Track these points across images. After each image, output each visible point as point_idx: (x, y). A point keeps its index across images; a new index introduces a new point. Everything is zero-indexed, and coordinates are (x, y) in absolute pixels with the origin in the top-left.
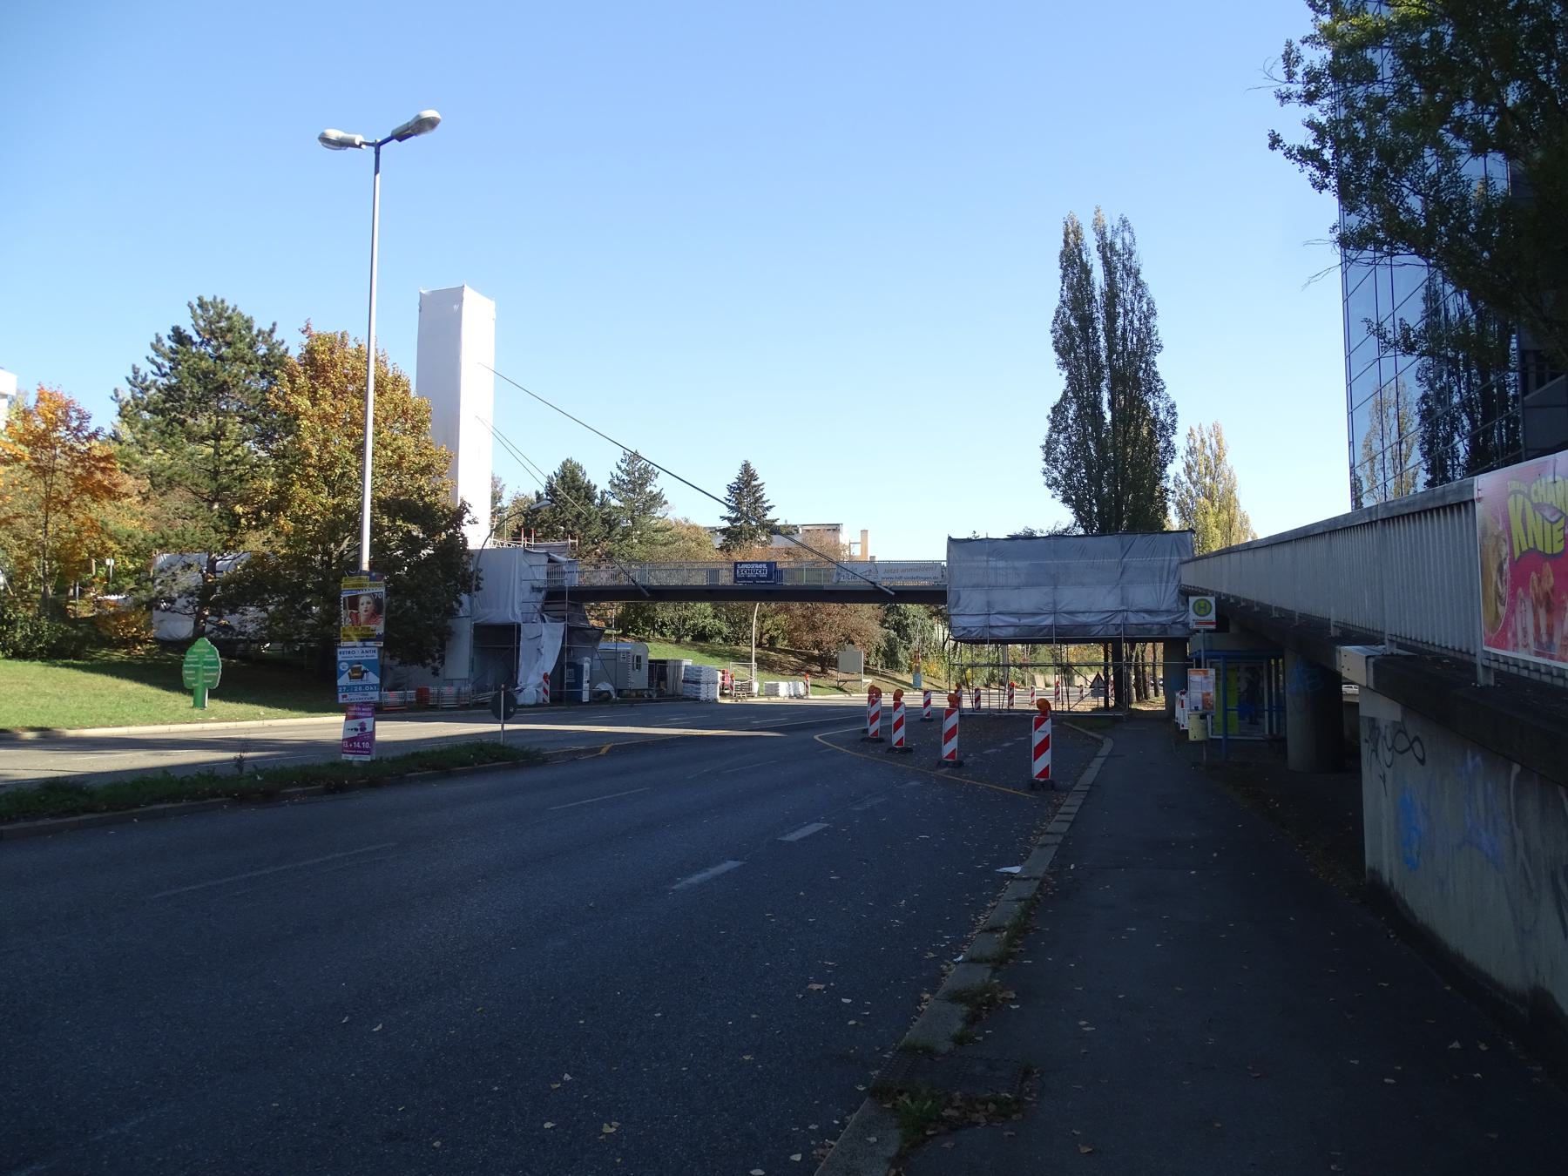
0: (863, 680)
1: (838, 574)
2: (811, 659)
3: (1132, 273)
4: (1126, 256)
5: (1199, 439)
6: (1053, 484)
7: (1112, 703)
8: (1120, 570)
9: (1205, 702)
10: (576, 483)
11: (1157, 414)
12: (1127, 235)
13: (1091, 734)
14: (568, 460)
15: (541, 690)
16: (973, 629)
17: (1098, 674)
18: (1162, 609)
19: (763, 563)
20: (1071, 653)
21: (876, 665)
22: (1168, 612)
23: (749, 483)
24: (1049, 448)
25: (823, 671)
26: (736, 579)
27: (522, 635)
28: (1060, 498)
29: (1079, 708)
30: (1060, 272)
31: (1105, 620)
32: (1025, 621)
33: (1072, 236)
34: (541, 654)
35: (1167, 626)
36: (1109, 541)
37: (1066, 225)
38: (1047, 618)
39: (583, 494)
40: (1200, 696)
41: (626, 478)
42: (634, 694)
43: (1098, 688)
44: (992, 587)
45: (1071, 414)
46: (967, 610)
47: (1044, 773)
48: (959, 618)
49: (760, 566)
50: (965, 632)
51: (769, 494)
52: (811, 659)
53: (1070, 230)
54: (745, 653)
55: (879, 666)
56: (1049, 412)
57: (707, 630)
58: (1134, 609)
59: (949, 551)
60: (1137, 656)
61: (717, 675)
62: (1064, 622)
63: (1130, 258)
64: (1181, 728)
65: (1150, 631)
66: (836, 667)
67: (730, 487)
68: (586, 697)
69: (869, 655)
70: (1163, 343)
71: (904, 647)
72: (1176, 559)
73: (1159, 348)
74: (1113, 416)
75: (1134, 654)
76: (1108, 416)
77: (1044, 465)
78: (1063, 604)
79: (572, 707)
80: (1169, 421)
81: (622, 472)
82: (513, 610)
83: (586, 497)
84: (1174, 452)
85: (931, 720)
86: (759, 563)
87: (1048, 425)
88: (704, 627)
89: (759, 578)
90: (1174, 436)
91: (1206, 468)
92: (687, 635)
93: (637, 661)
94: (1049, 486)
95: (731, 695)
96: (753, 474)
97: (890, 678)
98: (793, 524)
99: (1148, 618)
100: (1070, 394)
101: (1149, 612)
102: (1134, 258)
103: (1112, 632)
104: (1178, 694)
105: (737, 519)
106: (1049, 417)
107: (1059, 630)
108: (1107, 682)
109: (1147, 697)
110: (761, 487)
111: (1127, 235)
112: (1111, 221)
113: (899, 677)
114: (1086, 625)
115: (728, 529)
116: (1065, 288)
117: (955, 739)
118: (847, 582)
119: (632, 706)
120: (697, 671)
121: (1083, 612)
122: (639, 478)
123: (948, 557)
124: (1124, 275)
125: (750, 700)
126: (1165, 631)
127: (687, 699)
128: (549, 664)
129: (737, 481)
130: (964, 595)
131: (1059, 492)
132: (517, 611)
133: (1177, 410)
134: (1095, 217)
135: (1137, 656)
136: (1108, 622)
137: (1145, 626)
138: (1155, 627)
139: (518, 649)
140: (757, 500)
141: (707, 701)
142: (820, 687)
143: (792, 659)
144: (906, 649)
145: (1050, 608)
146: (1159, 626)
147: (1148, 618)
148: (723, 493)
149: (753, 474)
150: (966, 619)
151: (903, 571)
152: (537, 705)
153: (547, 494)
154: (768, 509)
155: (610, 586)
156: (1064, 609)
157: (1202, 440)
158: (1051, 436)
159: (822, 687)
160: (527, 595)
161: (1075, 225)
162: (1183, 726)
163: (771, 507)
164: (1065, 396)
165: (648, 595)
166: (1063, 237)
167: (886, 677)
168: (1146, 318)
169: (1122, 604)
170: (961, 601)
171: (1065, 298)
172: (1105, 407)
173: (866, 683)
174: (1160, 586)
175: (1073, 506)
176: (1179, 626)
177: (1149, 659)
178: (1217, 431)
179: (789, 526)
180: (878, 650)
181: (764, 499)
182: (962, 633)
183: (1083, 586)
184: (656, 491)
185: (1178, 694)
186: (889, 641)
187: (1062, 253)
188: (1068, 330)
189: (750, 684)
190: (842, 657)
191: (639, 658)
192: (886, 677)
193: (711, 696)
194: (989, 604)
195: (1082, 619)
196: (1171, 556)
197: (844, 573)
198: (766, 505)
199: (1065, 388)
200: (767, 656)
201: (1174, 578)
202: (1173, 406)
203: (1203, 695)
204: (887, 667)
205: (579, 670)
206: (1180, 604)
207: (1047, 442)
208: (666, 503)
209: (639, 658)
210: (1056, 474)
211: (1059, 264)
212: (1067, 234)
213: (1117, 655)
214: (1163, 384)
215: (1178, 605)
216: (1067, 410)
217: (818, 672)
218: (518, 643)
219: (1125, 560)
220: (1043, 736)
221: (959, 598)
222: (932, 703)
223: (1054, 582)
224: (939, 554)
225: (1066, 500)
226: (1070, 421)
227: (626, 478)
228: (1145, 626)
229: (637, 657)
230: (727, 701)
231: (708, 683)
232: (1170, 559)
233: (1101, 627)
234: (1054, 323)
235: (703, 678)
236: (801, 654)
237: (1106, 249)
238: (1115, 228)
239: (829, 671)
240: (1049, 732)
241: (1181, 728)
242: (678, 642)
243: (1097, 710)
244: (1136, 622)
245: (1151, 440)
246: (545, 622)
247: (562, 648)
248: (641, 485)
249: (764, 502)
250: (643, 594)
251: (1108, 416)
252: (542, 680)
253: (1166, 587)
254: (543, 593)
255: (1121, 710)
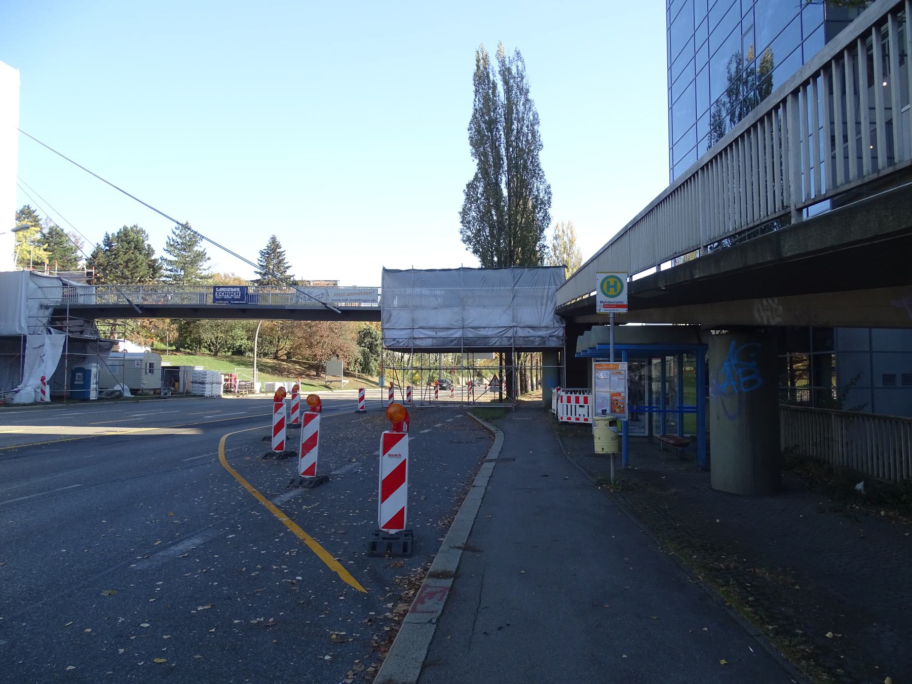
0: (343, 381)
1: (297, 296)
2: (311, 367)
3: (524, 92)
4: (519, 79)
5: (561, 230)
6: (468, 240)
7: (504, 396)
8: (512, 296)
9: (614, 403)
10: (128, 238)
11: (539, 193)
12: (520, 64)
13: (486, 425)
14: (134, 226)
15: (39, 390)
16: (401, 340)
17: (495, 376)
18: (542, 326)
19: (237, 287)
20: (480, 361)
21: (354, 371)
22: (547, 327)
23: (275, 250)
24: (465, 213)
25: (318, 375)
26: (215, 300)
27: (27, 345)
28: (471, 250)
29: (483, 399)
30: (473, 88)
31: (499, 334)
32: (441, 334)
33: (482, 61)
34: (43, 361)
35: (545, 338)
36: (505, 274)
37: (478, 53)
38: (457, 332)
39: (134, 246)
40: (608, 395)
41: (179, 240)
42: (152, 392)
43: (495, 385)
44: (416, 307)
45: (480, 190)
46: (396, 325)
47: (397, 520)
48: (390, 332)
49: (235, 290)
50: (395, 342)
51: (288, 258)
52: (311, 367)
53: (481, 57)
54: (264, 362)
55: (357, 371)
56: (465, 188)
57: (243, 348)
58: (521, 325)
59: (383, 279)
60: (522, 364)
61: (221, 376)
62: (470, 335)
63: (522, 81)
64: (560, 420)
65: (533, 342)
66: (325, 372)
67: (261, 252)
68: (93, 395)
69: (349, 364)
70: (544, 144)
71: (375, 359)
72: (553, 287)
73: (541, 147)
74: (509, 192)
75: (520, 362)
76: (505, 192)
77: (461, 226)
78: (470, 321)
79: (71, 405)
80: (546, 198)
81: (177, 236)
82: (20, 324)
83: (135, 248)
84: (550, 219)
85: (365, 412)
86: (233, 287)
87: (464, 197)
88: (241, 346)
89: (233, 299)
90: (549, 209)
91: (564, 248)
92: (229, 351)
93: (150, 367)
94: (464, 241)
95: (234, 392)
96: (278, 245)
97: (364, 379)
98: (308, 280)
99: (532, 333)
100: (480, 176)
101: (533, 328)
102: (524, 81)
103: (505, 343)
104: (555, 391)
105: (265, 274)
106: (464, 191)
107: (466, 341)
108: (501, 381)
109: (526, 391)
110: (283, 253)
111: (520, 64)
112: (509, 53)
113: (370, 378)
114: (486, 338)
115: (260, 280)
116: (477, 100)
117: (315, 451)
118: (304, 303)
119: (137, 402)
120: (203, 375)
121: (484, 328)
122: (189, 241)
123: (383, 284)
124: (518, 93)
125: (251, 396)
126: (544, 342)
127: (195, 396)
128: (49, 369)
129: (267, 248)
130: (394, 313)
131: (470, 246)
132: (23, 324)
133: (552, 190)
134: (498, 49)
135: (522, 364)
136: (501, 335)
137: (530, 338)
138: (537, 339)
139: (24, 357)
140: (280, 262)
141: (212, 397)
142: (313, 385)
143: (298, 367)
144: (376, 360)
145: (459, 324)
146: (539, 339)
147: (532, 333)
148: (255, 257)
149: (278, 245)
150: (395, 332)
151: (348, 295)
152: (35, 403)
153: (106, 245)
154: (287, 268)
155: (99, 305)
156: (471, 325)
157: (563, 231)
158: (466, 205)
159: (315, 386)
160: (35, 312)
161: (484, 54)
162: (562, 418)
163: (289, 267)
164: (476, 177)
165: (140, 312)
166: (476, 62)
167: (362, 378)
168: (532, 125)
169: (513, 321)
170: (392, 318)
171: (477, 107)
172: (503, 186)
173: (344, 383)
174: (541, 308)
175: (480, 256)
176: (554, 339)
177: (528, 364)
178: (570, 227)
179: (304, 281)
180: (356, 361)
181: (285, 261)
182: (393, 343)
183: (485, 307)
184: (201, 250)
185: (555, 391)
186: (364, 354)
187: (475, 74)
188: (479, 131)
189: (252, 384)
190: (328, 365)
191: (151, 365)
192: (362, 378)
193: (215, 393)
194: (413, 320)
195: (483, 332)
196: (549, 286)
197: (302, 296)
198: (286, 265)
199: (476, 171)
200: (280, 365)
201: (551, 302)
202: (549, 187)
203: (613, 395)
204: (363, 372)
205: (87, 374)
206: (555, 322)
207: (463, 209)
208: (209, 259)
209: (151, 365)
210: (469, 233)
211: (473, 82)
212: (478, 61)
213: (509, 361)
214: (543, 172)
215: (554, 323)
216: (477, 187)
217: (314, 376)
218: (24, 351)
219: (515, 288)
220: (396, 463)
221: (391, 315)
222: (365, 397)
223: (462, 304)
224: (375, 281)
225: (475, 251)
226: (479, 196)
227: (179, 240)
228: (530, 338)
229: (150, 364)
230: (230, 397)
231: (212, 383)
232: (549, 288)
233: (497, 339)
234: (470, 124)
235: (208, 380)
236: (304, 363)
237: (506, 73)
238: (511, 58)
239: (322, 375)
240: (405, 455)
241: (560, 420)
242: (215, 355)
243: (493, 401)
244: (523, 335)
245: (534, 212)
246: (51, 333)
247: (63, 356)
248: (190, 245)
249: (284, 263)
250: (137, 312)
251: (505, 192)
252: (40, 382)
253: (546, 308)
254: (50, 310)
255: (510, 401)
